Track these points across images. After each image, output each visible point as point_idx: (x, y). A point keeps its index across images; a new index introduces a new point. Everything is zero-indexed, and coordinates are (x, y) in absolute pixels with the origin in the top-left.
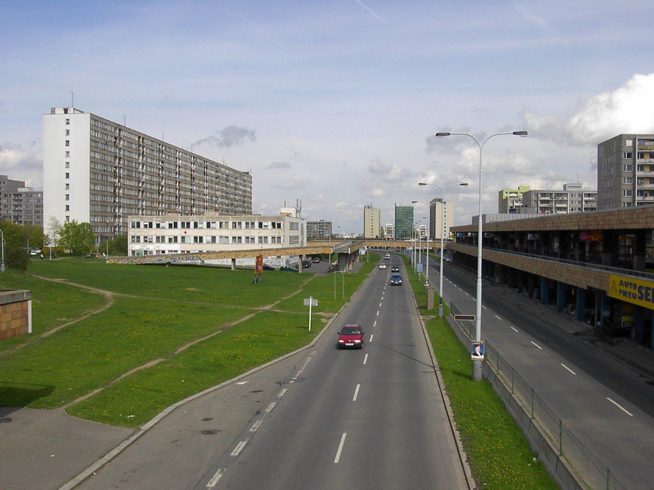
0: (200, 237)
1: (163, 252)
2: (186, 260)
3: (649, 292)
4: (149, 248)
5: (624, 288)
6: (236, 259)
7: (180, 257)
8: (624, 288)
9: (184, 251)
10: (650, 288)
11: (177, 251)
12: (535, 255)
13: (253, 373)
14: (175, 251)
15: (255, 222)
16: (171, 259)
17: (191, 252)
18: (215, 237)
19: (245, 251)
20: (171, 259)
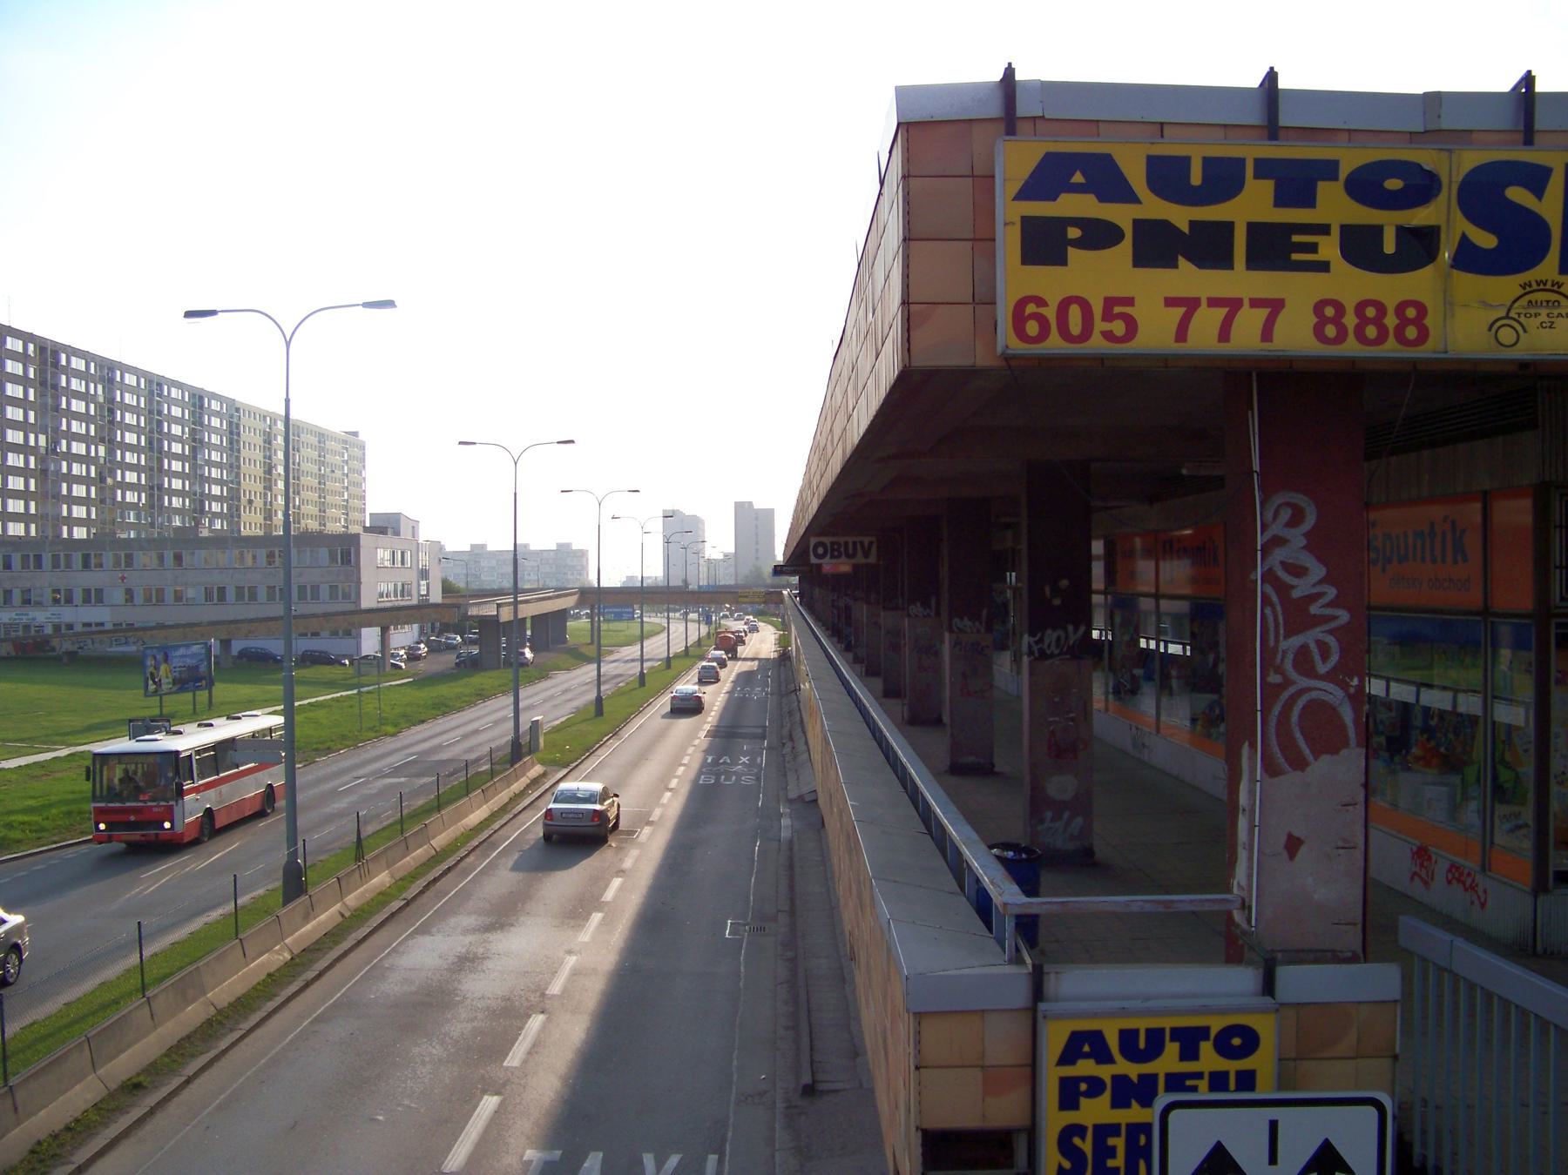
0: (312, 587)
1: (70, 627)
2: (111, 646)
3: (1111, 1141)
4: (34, 619)
5: (1439, 559)
6: (233, 642)
7: (94, 637)
8: (1439, 559)
9: (121, 624)
10: (1118, 1126)
11: (102, 624)
12: (240, 715)
13: (191, 963)
14: (97, 624)
15: (44, 555)
16: (73, 644)
17: (136, 626)
18: (102, 590)
19: (251, 621)
20: (73, 644)
